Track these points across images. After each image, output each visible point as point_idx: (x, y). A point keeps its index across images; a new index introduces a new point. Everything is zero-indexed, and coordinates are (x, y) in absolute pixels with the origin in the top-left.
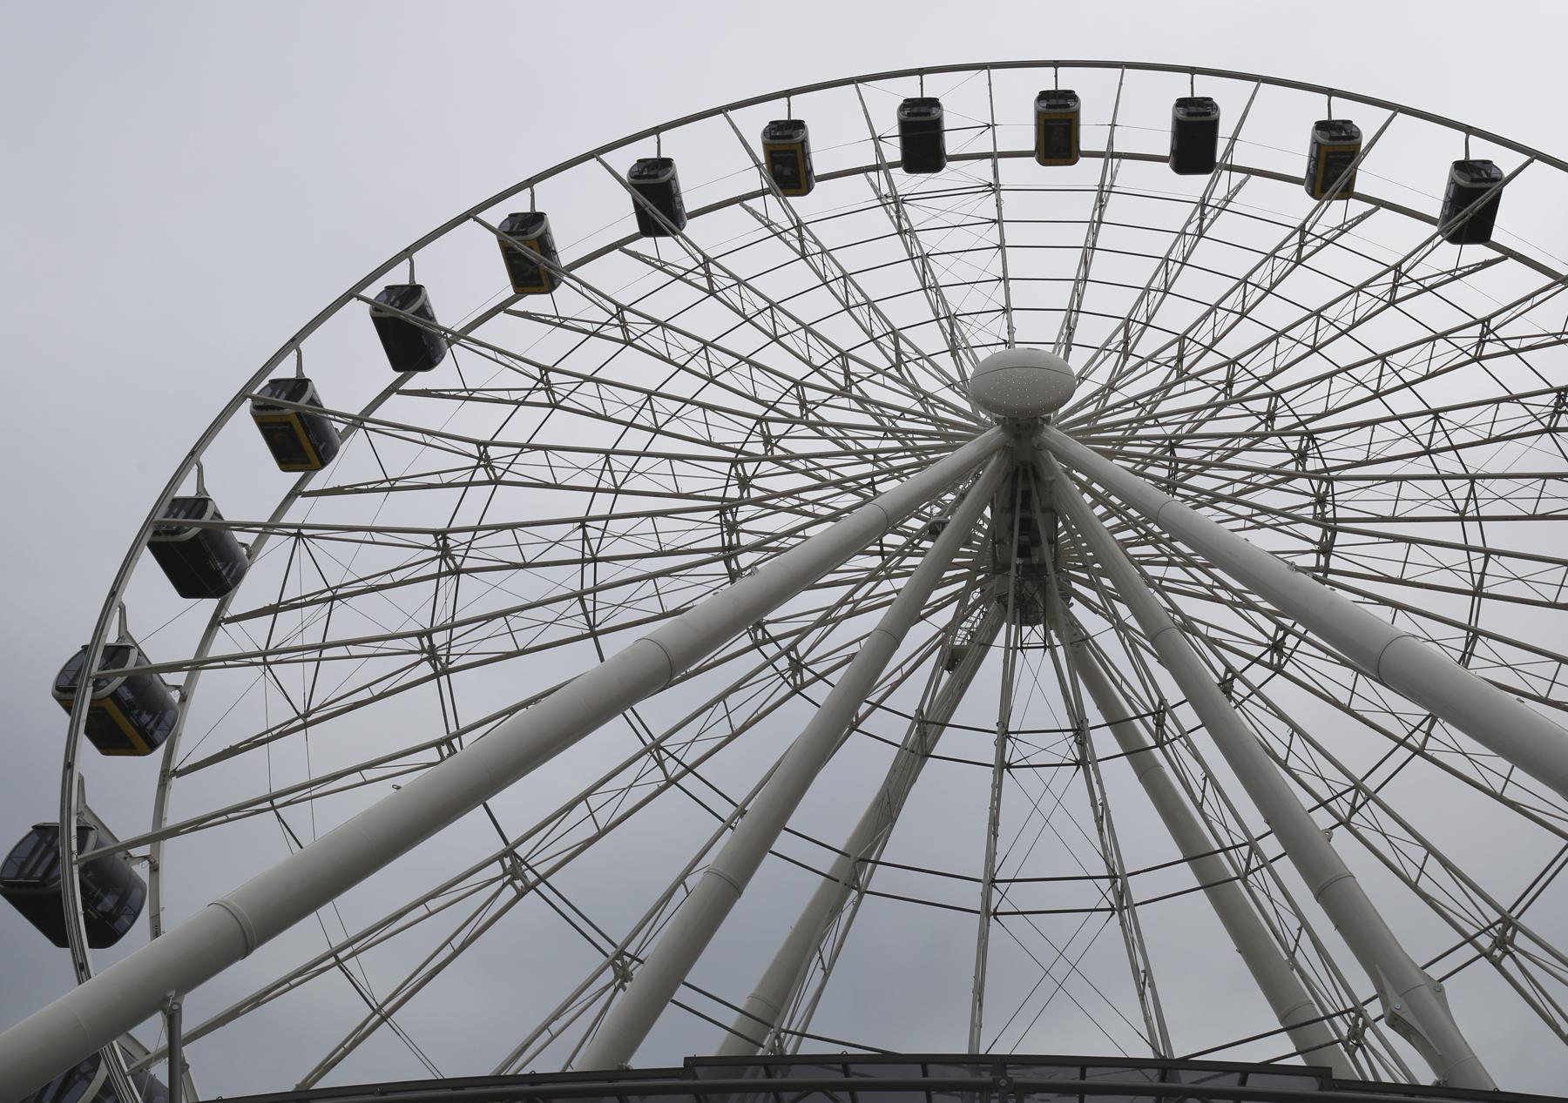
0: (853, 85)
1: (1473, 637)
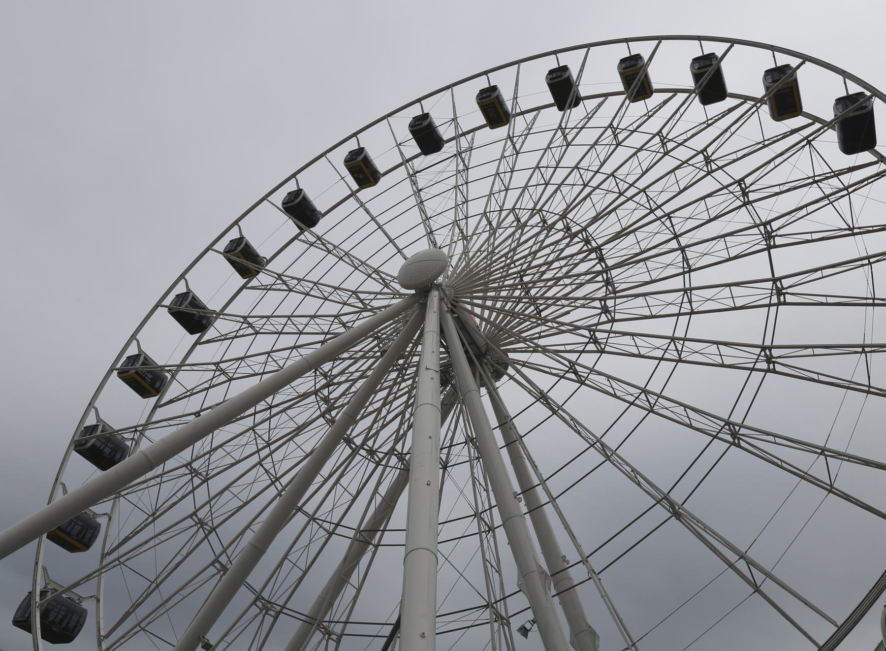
0: (265, 201)
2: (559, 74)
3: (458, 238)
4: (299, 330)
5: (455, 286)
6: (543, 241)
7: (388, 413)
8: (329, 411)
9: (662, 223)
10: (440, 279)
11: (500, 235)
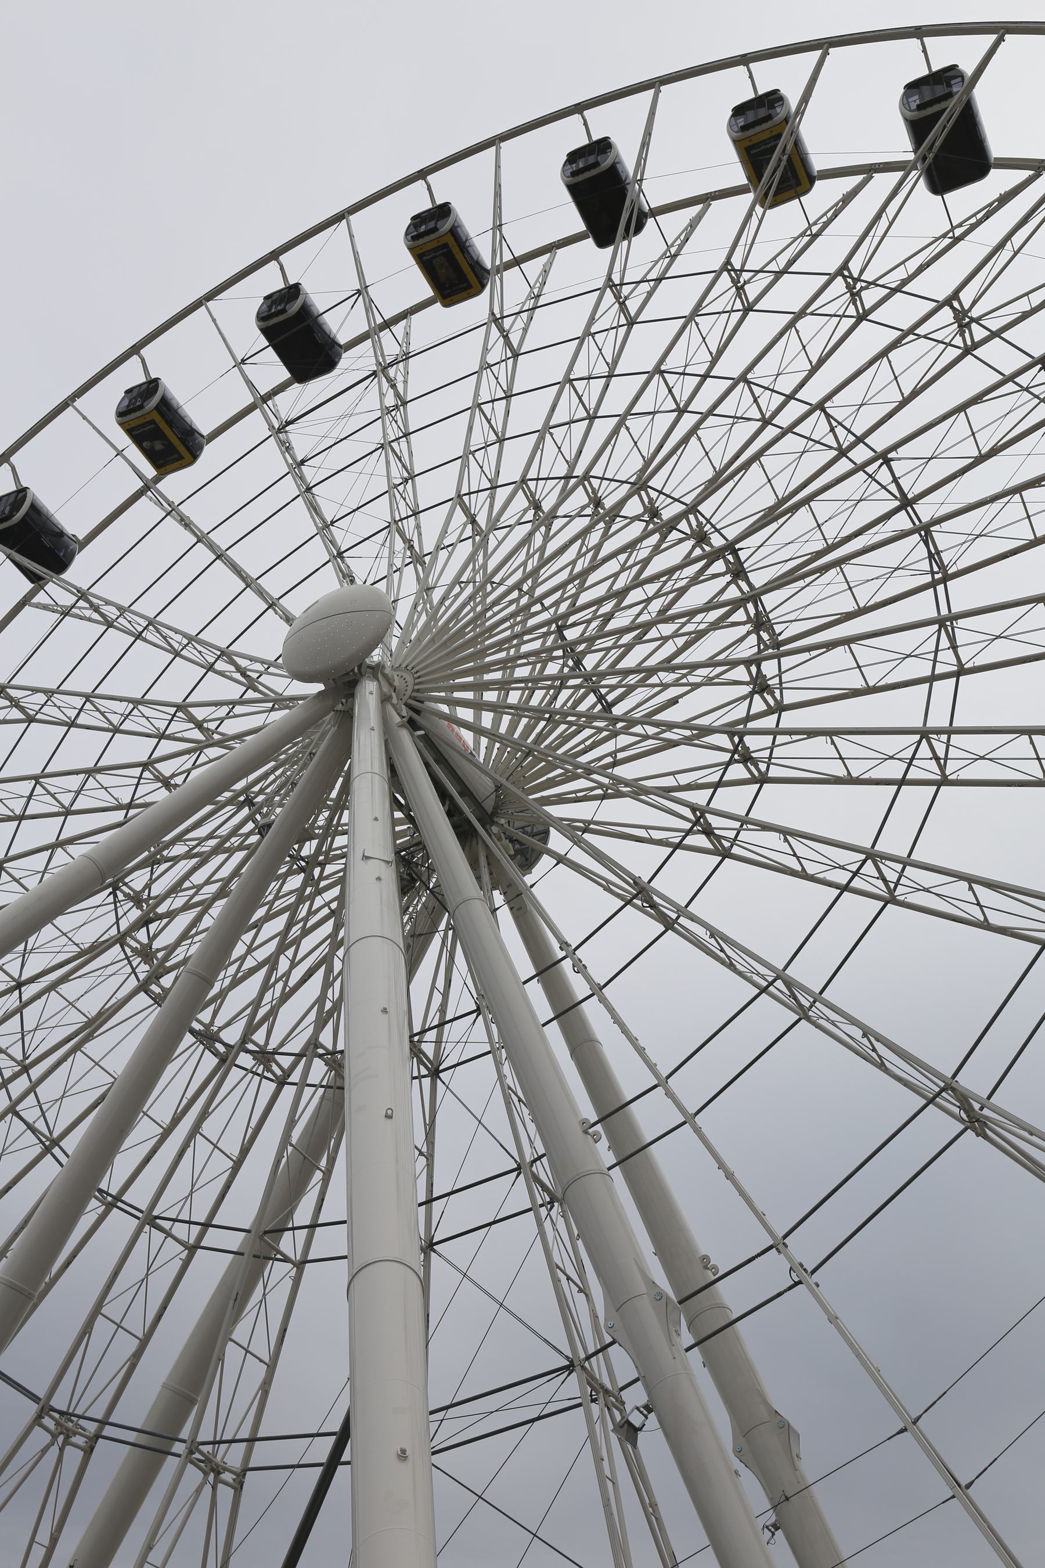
1: (926, 535)
2: (591, 159)
3: (403, 560)
4: (63, 806)
5: (412, 665)
6: (598, 547)
7: (293, 965)
8: (155, 976)
9: (870, 476)
10: (376, 656)
11: (500, 543)
